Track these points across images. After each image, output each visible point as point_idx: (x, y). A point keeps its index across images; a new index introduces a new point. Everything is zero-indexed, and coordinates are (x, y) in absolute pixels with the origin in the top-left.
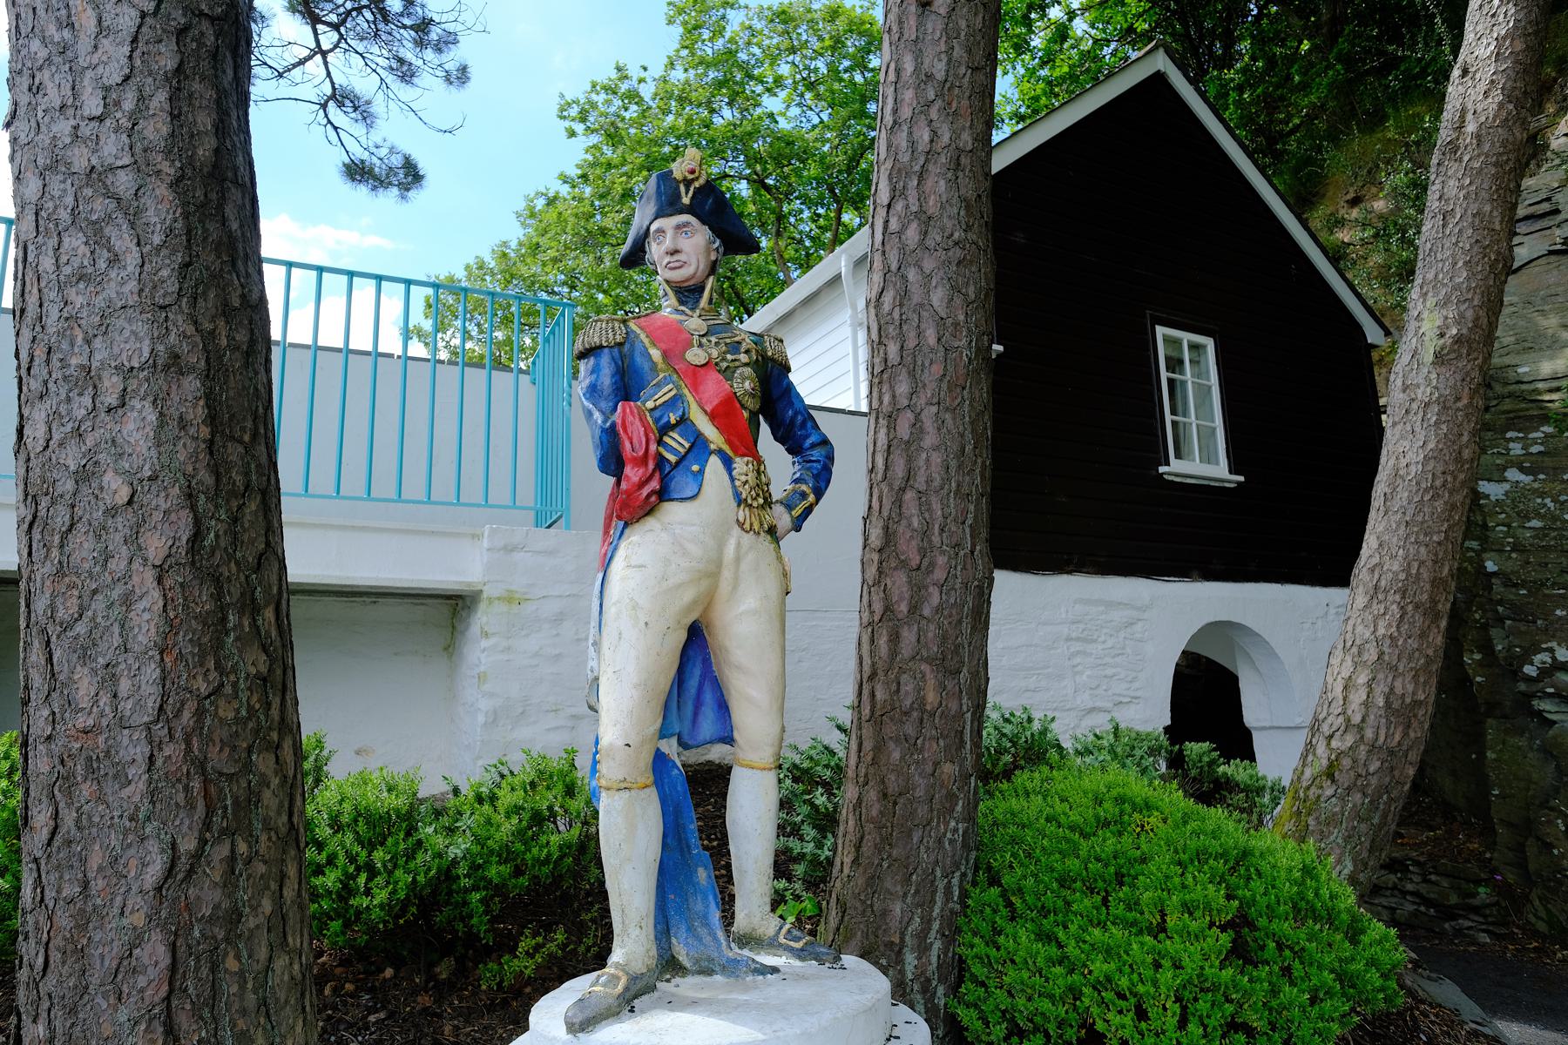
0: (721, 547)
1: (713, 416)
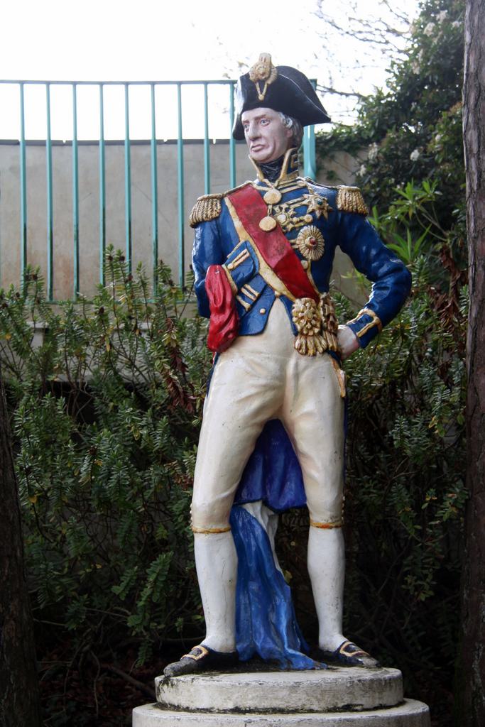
0: (283, 367)
1: (276, 270)
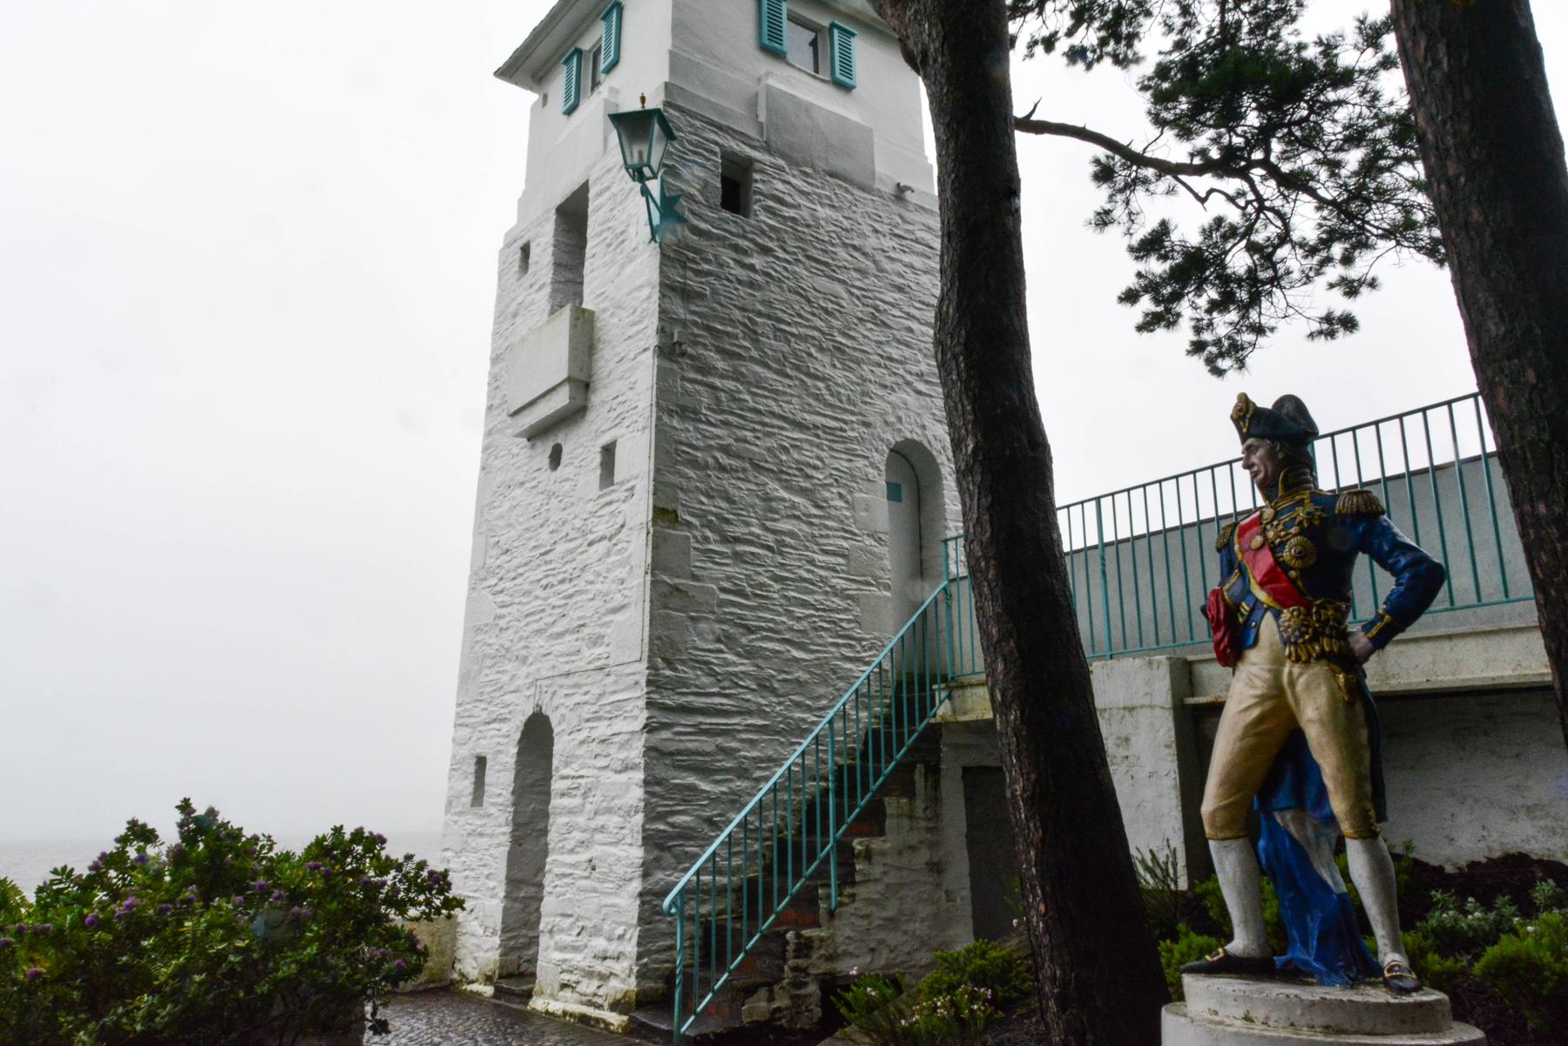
0: (1277, 675)
